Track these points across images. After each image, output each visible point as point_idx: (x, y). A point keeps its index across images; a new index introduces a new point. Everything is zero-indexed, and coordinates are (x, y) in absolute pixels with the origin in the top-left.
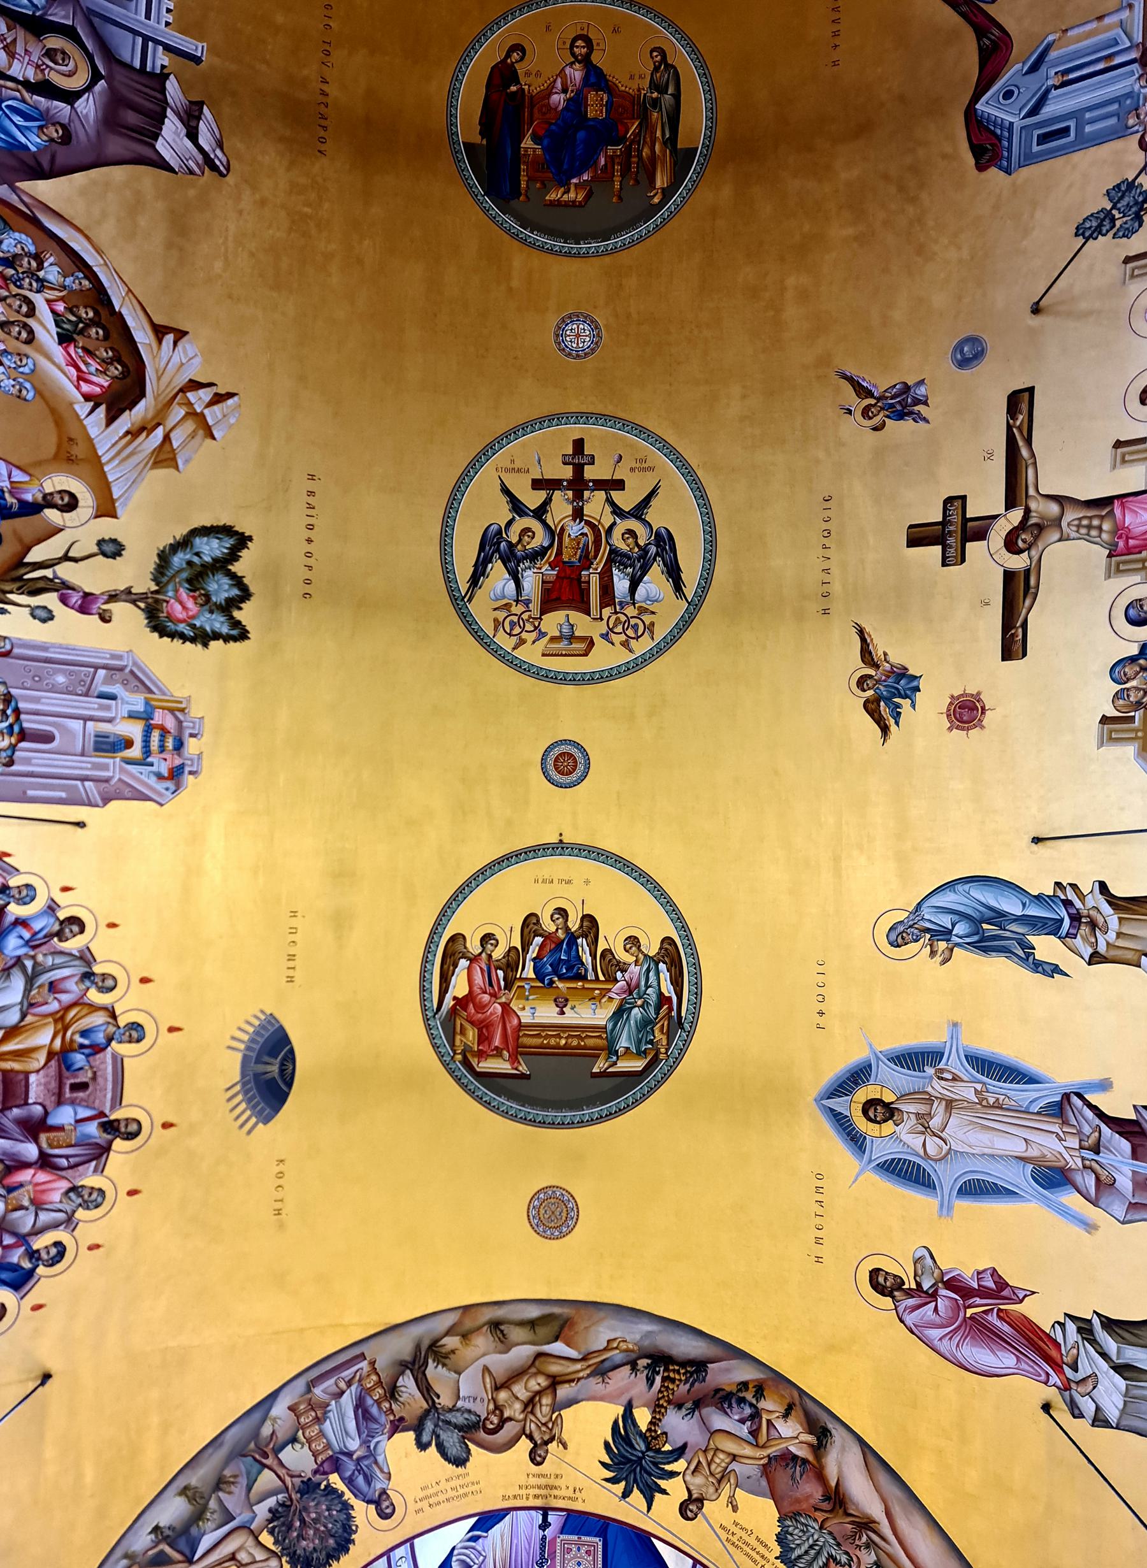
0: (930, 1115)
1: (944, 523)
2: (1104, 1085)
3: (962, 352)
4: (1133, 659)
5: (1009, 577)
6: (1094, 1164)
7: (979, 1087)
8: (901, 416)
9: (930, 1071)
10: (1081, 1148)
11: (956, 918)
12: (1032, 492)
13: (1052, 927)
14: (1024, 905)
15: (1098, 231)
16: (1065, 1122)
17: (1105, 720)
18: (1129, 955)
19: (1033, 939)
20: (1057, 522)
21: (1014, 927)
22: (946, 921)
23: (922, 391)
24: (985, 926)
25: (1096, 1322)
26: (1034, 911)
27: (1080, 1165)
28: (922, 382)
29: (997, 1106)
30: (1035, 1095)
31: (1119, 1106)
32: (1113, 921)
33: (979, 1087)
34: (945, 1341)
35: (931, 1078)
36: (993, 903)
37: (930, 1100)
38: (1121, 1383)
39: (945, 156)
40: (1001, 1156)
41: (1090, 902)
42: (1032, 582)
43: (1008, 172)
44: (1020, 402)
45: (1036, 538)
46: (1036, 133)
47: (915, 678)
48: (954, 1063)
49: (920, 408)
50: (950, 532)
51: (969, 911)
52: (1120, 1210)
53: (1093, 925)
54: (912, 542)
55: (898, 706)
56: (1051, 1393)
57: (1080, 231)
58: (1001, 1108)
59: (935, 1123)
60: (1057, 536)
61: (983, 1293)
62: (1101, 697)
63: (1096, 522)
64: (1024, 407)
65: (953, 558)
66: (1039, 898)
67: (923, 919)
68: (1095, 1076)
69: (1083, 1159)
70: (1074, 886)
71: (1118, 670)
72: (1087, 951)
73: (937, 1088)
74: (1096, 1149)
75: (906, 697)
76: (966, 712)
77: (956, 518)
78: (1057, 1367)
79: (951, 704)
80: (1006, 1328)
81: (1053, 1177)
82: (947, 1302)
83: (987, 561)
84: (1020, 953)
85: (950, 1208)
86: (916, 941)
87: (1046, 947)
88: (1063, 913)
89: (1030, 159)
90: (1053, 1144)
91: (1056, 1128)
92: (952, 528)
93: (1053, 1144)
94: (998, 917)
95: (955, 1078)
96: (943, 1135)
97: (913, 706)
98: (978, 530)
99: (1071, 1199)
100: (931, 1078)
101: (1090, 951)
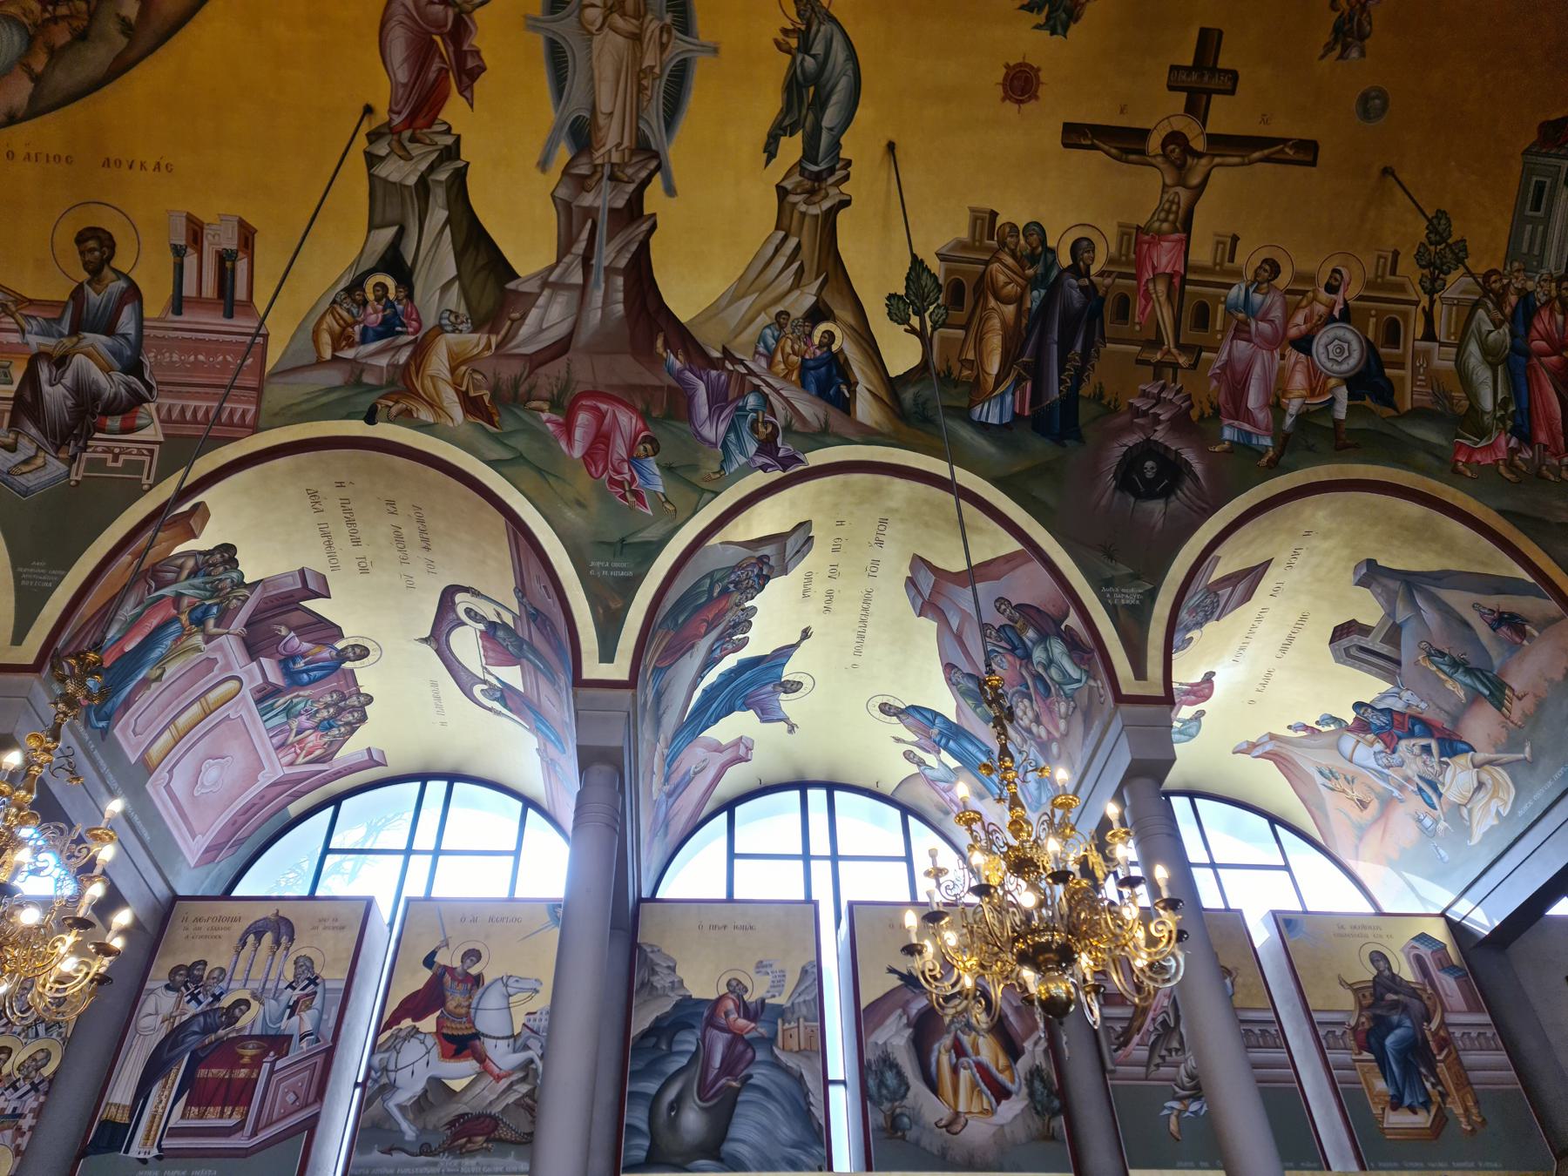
0: (623, 15)
1: (1214, 70)
2: (670, 190)
3: (1377, 97)
4: (1043, 241)
5: (1143, 134)
6: (598, 176)
7: (657, 70)
8: (1337, 30)
9: (668, 19)
10: (613, 165)
11: (821, 58)
12: (1217, 160)
13: (810, 153)
14: (831, 129)
15: (1432, 228)
16: (633, 152)
17: (994, 215)
18: (786, 222)
19: (799, 136)
20: (1181, 182)
21: (810, 118)
22: (818, 49)
23: (1354, 54)
24: (812, 89)
25: (460, 164)
26: (825, 138)
27: (599, 161)
28: (1363, 54)
29: (641, 89)
30: (654, 125)
31: (654, 198)
32: (814, 210)
33: (657, 70)
34: (401, 9)
35: (661, 19)
36: (834, 99)
37: (639, 16)
38: (412, 181)
39: (222, 1112)
40: (593, 87)
41: (833, 191)
42: (1133, 157)
43: (1526, 152)
44: (1307, 152)
45: (1172, 163)
46: (1548, 181)
47: (1065, 29)
48: (678, 46)
49: (1339, 48)
50: (1202, 79)
51: (826, 74)
52: (563, 193)
53: (812, 192)
54: (1204, 34)
55: (1040, 10)
56: (382, 115)
57: (1441, 214)
58: (639, 92)
59: (617, 19)
60: (1168, 181)
61: (460, 56)
62: (1014, 213)
63: (1171, 217)
64: (1300, 157)
65: (1177, 78)
66: (836, 145)
67: (820, 23)
68: (678, 183)
69: (603, 165)
70: (847, 178)
71: (1036, 230)
72: (788, 185)
73: (653, 27)
74: (612, 178)
75: (1048, 18)
76: (1021, 84)
77: (1215, 83)
78: (410, 122)
79: (1032, 67)
80: (432, 76)
81: (582, 135)
82: (442, 15)
83: (1162, 112)
84: (786, 122)
85: (534, 28)
86: (798, 14)
87: (792, 148)
88: (823, 166)
89: (1527, 172)
90: (612, 139)
91: (626, 143)
92: (1206, 78)
93: (612, 139)
94: (820, 104)
95: (663, 47)
96: (606, 30)
97: (1038, 27)
98: (1197, 107)
99: (564, 153)
100: (661, 19)
101: (789, 187)
